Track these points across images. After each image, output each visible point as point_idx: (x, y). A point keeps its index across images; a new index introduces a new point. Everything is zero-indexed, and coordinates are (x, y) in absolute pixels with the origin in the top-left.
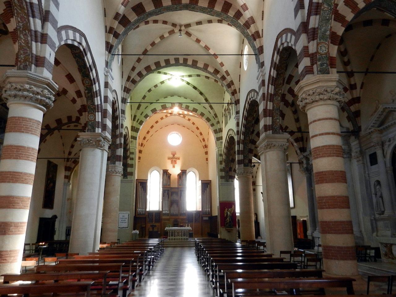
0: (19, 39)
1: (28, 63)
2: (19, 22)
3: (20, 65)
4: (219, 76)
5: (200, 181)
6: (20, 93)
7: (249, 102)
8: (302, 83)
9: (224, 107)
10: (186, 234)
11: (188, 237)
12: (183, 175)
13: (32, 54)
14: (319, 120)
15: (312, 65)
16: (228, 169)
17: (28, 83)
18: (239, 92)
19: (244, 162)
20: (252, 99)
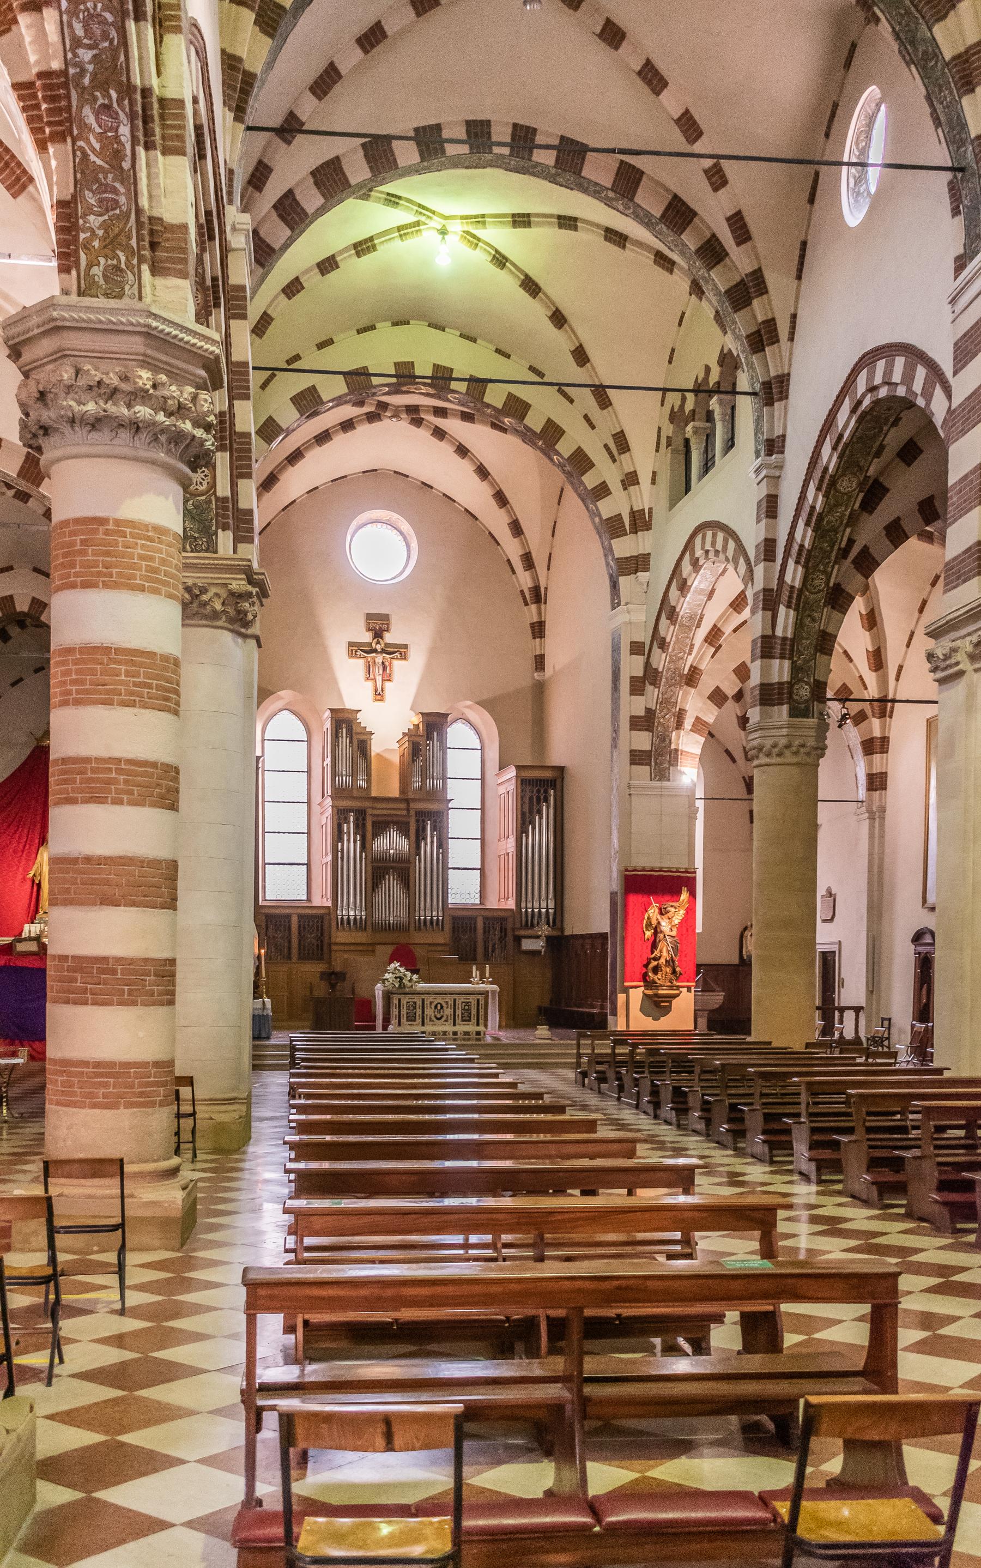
0: (75, 132)
1: (123, 259)
2: (77, 43)
3: (90, 266)
4: (691, 240)
7: (859, 403)
10: (474, 1012)
12: (429, 737)
13: (139, 211)
17: (145, 363)
18: (791, 339)
19: (790, 697)
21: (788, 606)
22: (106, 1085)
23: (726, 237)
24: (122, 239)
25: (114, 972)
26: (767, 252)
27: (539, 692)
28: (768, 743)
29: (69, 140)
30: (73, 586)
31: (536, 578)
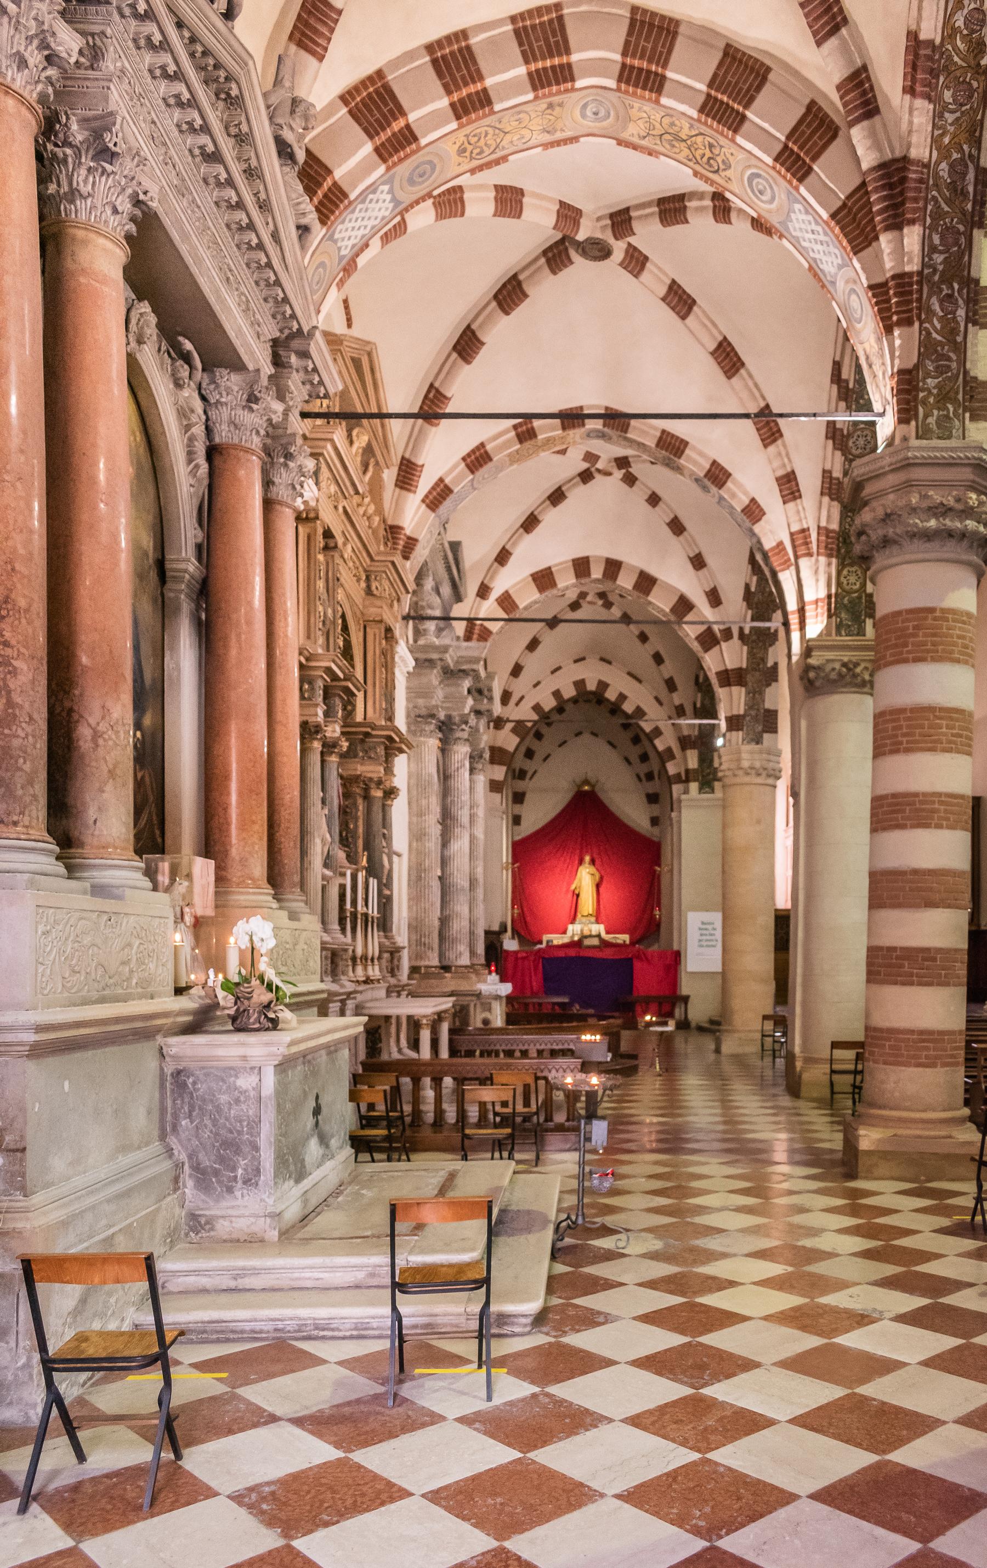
0: (923, 316)
2: (933, 249)
3: (926, 416)
22: (927, 1048)
24: (952, 394)
25: (934, 959)
29: (917, 324)
30: (906, 661)
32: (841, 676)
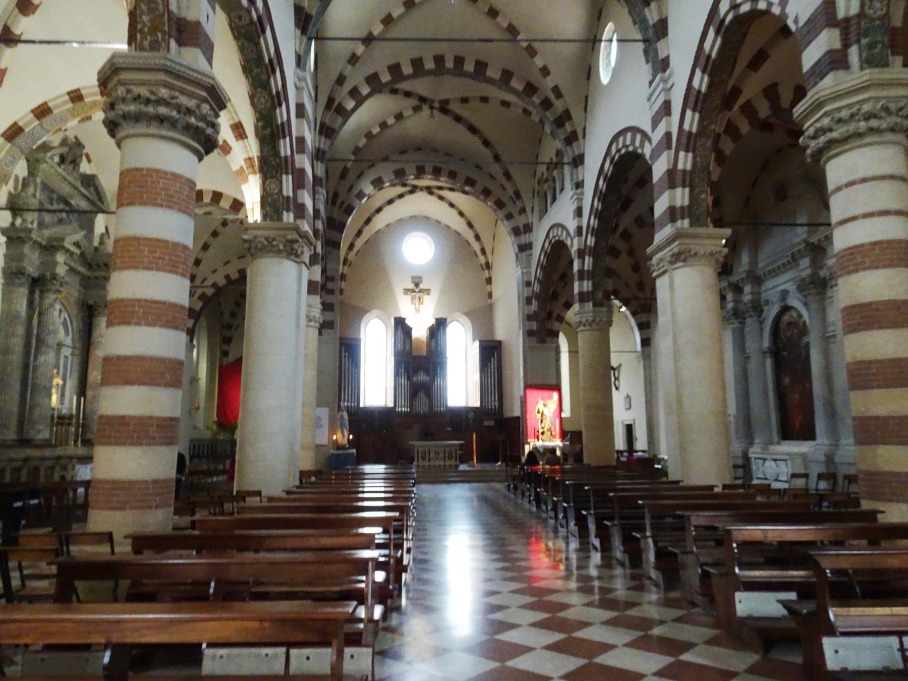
3: (142, 41)
4: (536, 100)
5: (477, 343)
6: (150, 109)
7: (614, 158)
8: (811, 96)
9: (538, 175)
11: (458, 463)
14: (864, 180)
15: (846, 45)
16: (544, 314)
17: (166, 85)
18: (584, 137)
20: (623, 151)
21: (589, 256)
23: (552, 97)
25: (128, 425)
26: (570, 101)
27: (491, 307)
28: (584, 320)
31: (486, 258)
32: (265, 247)
